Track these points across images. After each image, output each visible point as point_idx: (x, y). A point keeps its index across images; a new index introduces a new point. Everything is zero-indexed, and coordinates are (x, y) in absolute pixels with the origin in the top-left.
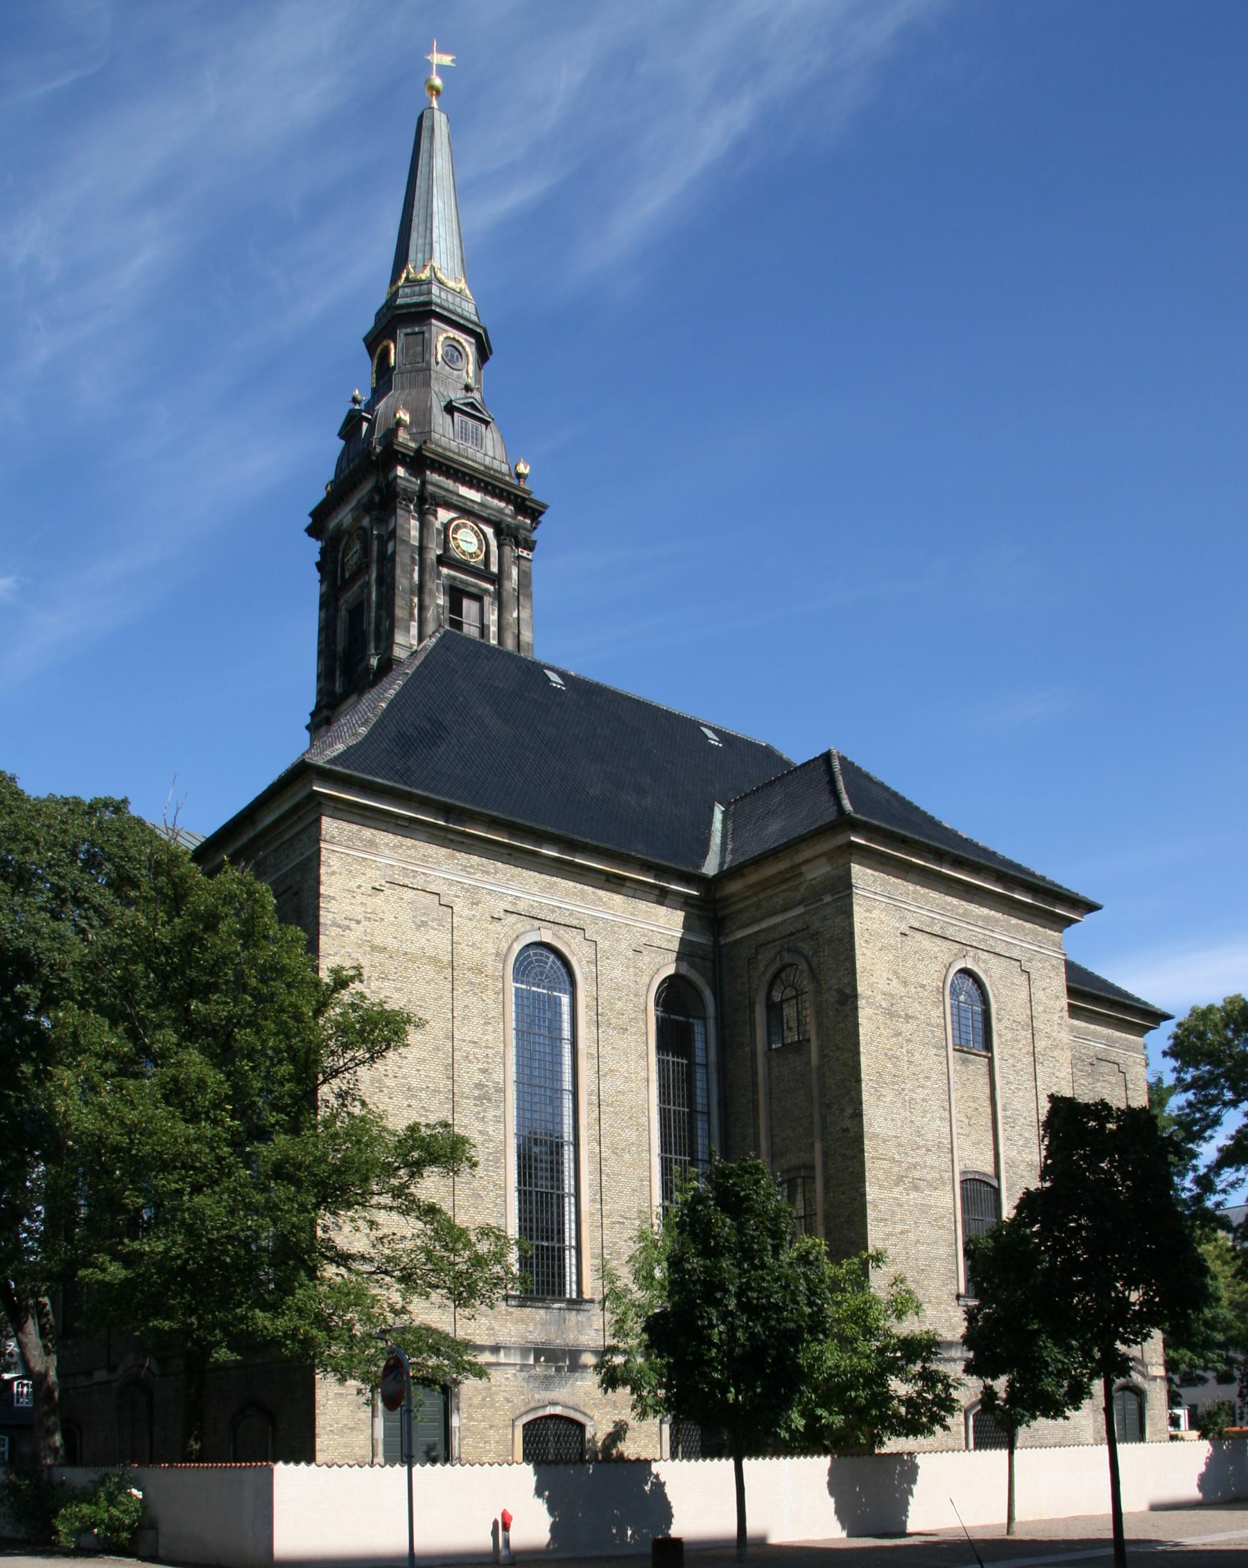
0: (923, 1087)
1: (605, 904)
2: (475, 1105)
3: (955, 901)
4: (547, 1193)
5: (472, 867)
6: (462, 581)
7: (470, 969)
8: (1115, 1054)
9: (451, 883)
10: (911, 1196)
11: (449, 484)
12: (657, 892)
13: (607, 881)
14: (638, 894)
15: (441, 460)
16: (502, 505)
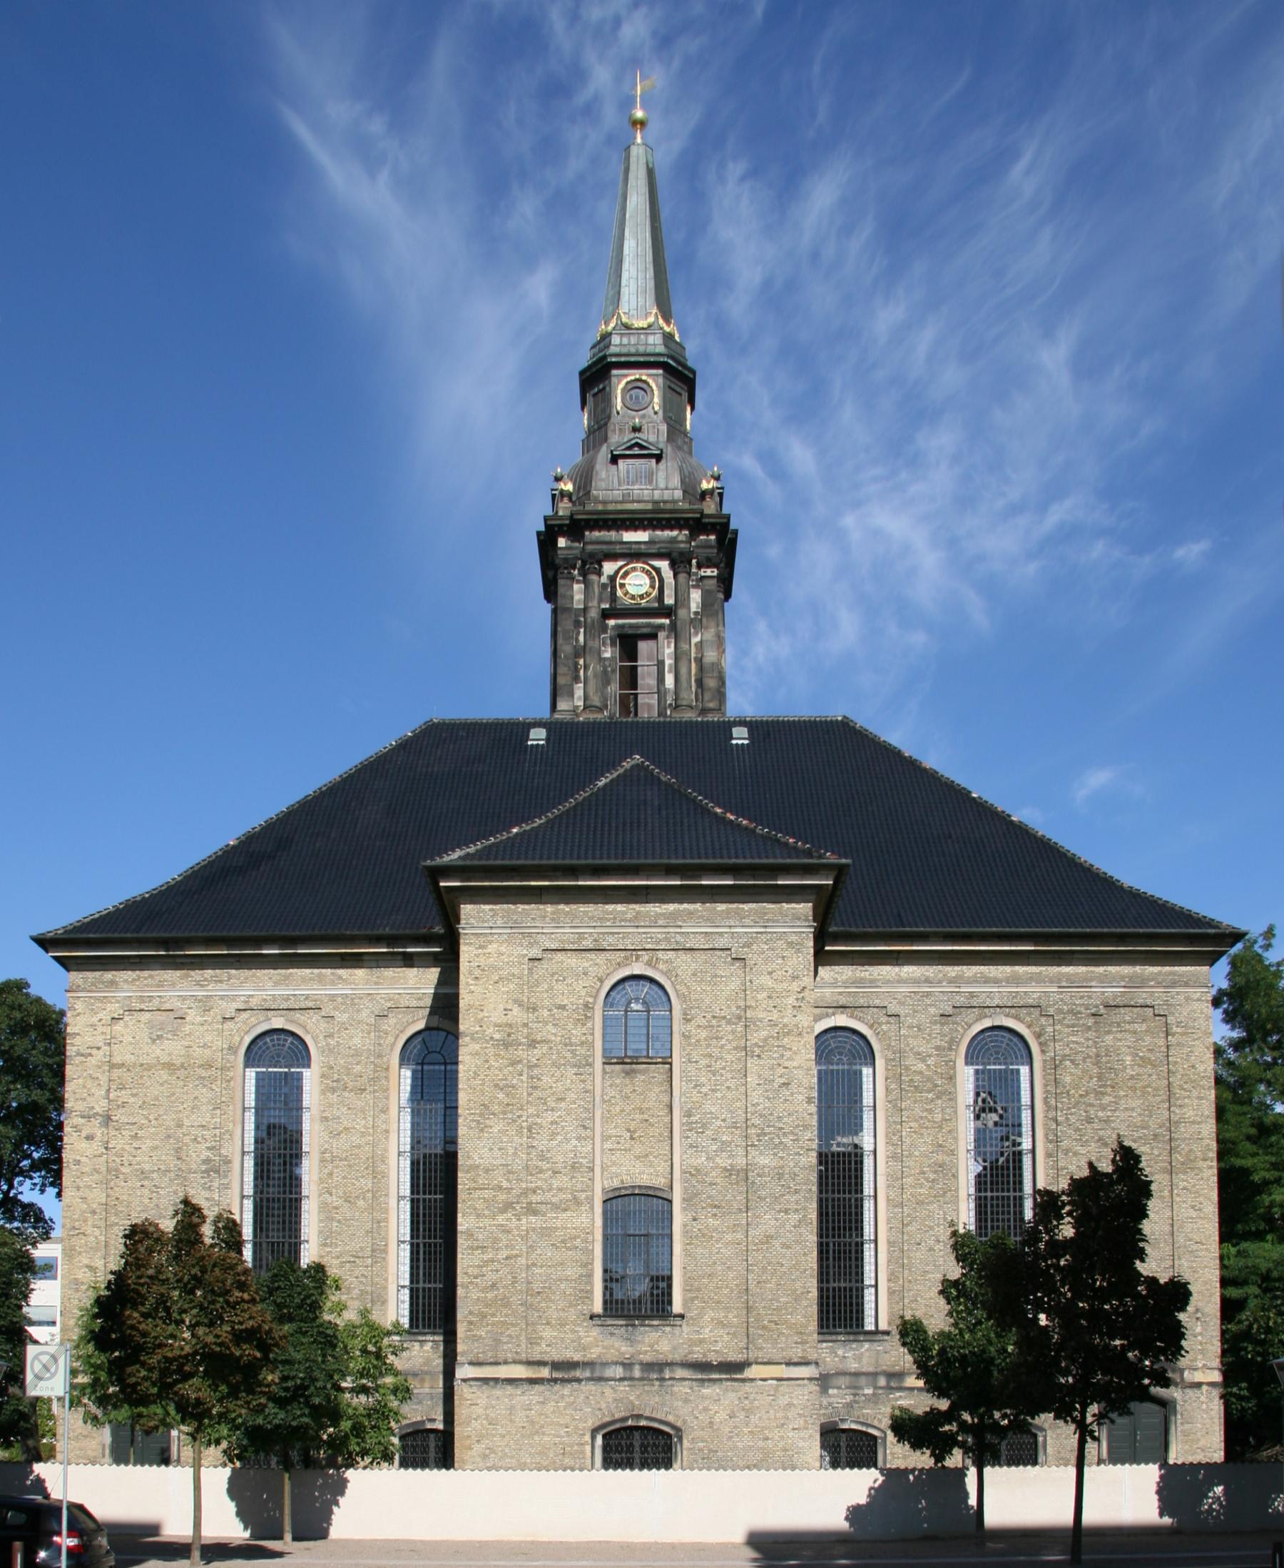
0: (552, 1110)
1: (344, 980)
2: (202, 1177)
3: (620, 907)
4: (278, 1243)
5: (206, 980)
6: (631, 626)
7: (200, 1067)
8: (1144, 995)
9: (184, 998)
10: (524, 1221)
11: (612, 535)
12: (400, 957)
13: (343, 960)
14: (380, 963)
15: (594, 517)
16: (675, 533)
